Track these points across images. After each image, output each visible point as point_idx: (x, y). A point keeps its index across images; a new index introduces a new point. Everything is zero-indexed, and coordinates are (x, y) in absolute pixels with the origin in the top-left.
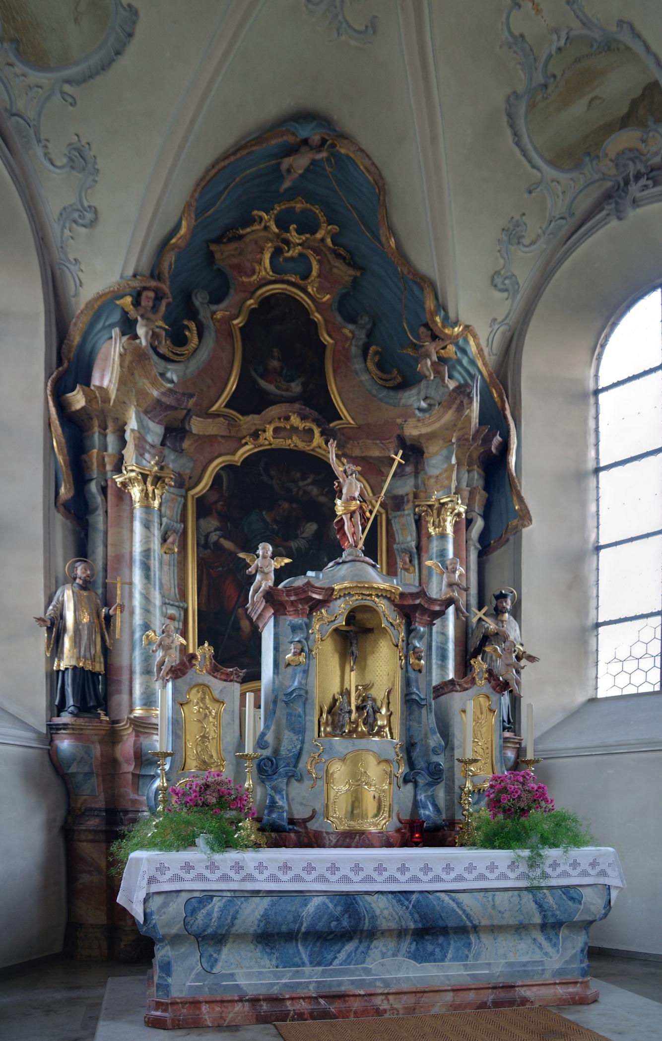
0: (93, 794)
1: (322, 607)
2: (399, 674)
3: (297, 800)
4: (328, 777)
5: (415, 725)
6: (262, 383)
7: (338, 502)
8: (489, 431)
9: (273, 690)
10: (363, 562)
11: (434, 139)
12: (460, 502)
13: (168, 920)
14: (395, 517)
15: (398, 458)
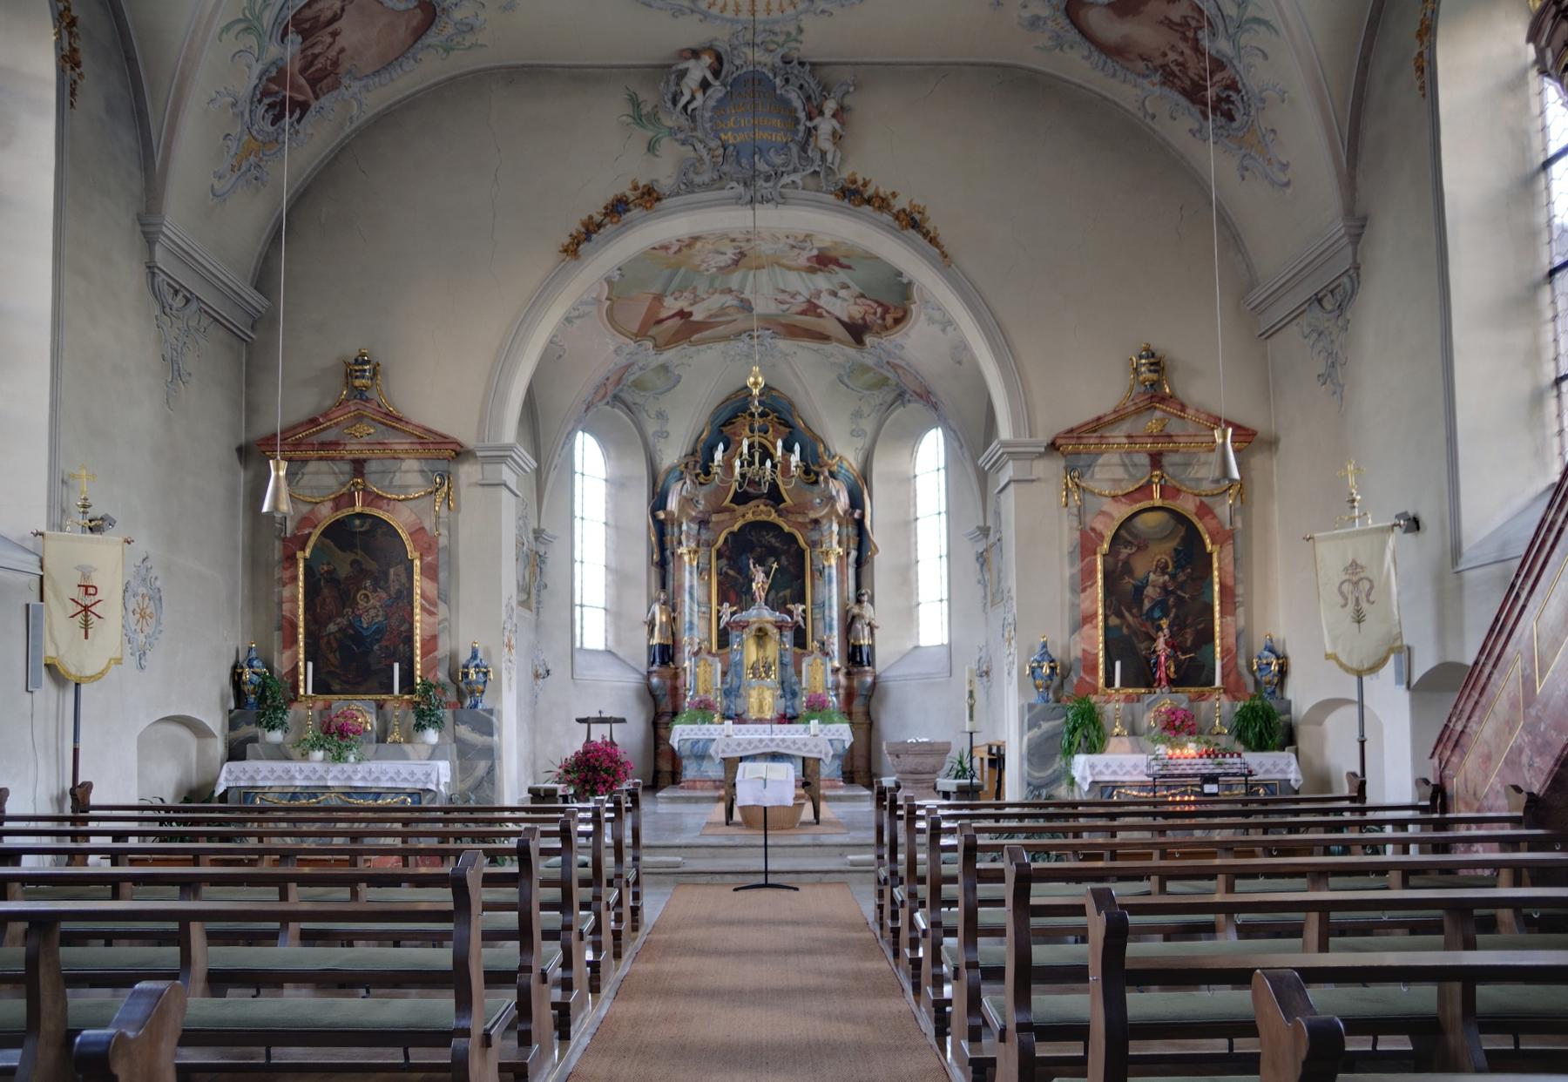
0: (666, 705)
3: (737, 706)
13: (685, 750)
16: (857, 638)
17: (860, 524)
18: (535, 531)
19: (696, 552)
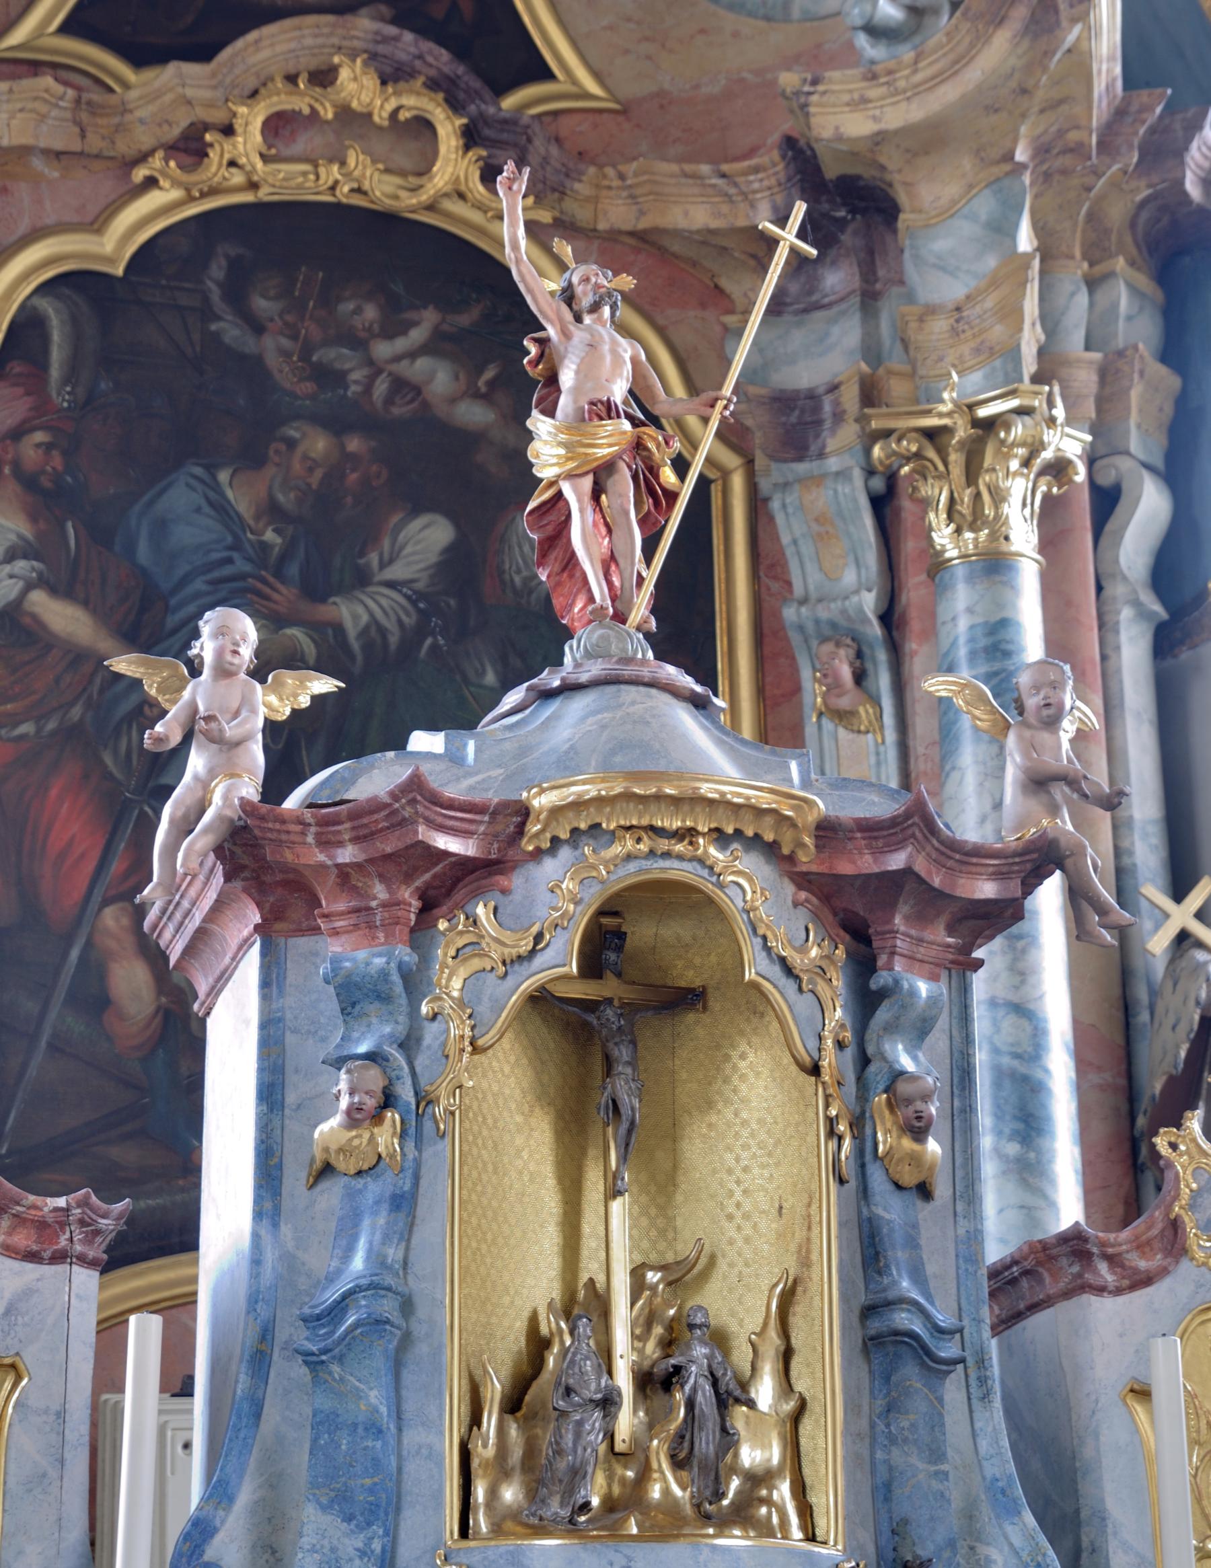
1: (477, 894)
2: (830, 1206)
5: (913, 1462)
7: (539, 424)
8: (1170, 109)
9: (253, 1300)
10: (652, 684)
12: (1059, 412)
14: (786, 486)
15: (789, 236)
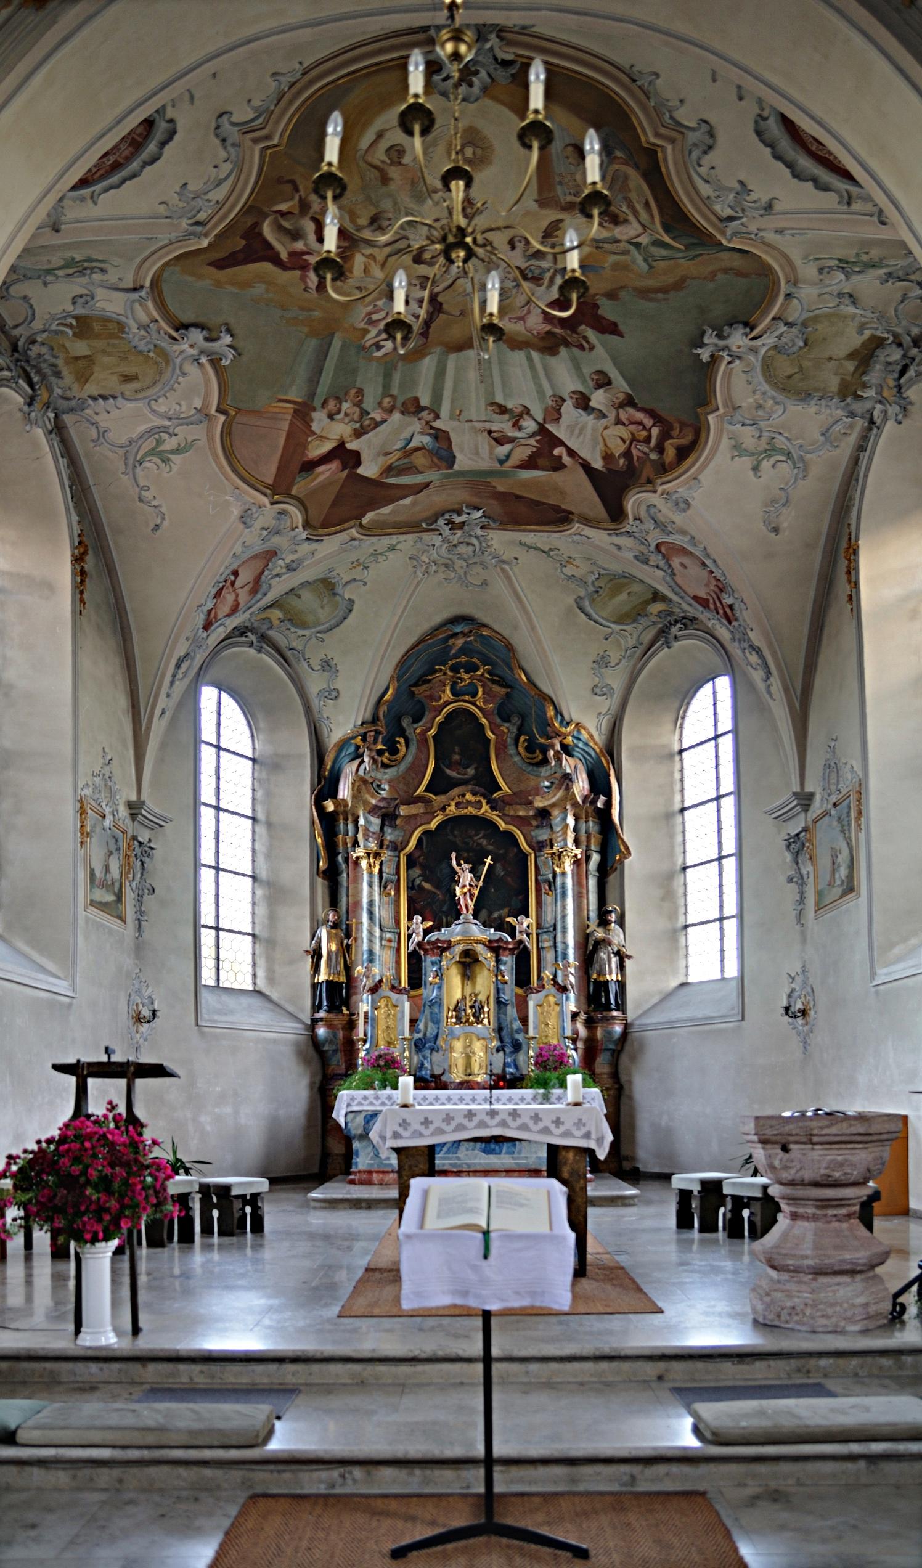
0: (338, 1062)
3: (434, 1064)
4: (451, 1049)
5: (502, 1016)
6: (448, 771)
11: (533, 628)
16: (601, 973)
17: (604, 817)
18: (130, 805)
19: (377, 855)
